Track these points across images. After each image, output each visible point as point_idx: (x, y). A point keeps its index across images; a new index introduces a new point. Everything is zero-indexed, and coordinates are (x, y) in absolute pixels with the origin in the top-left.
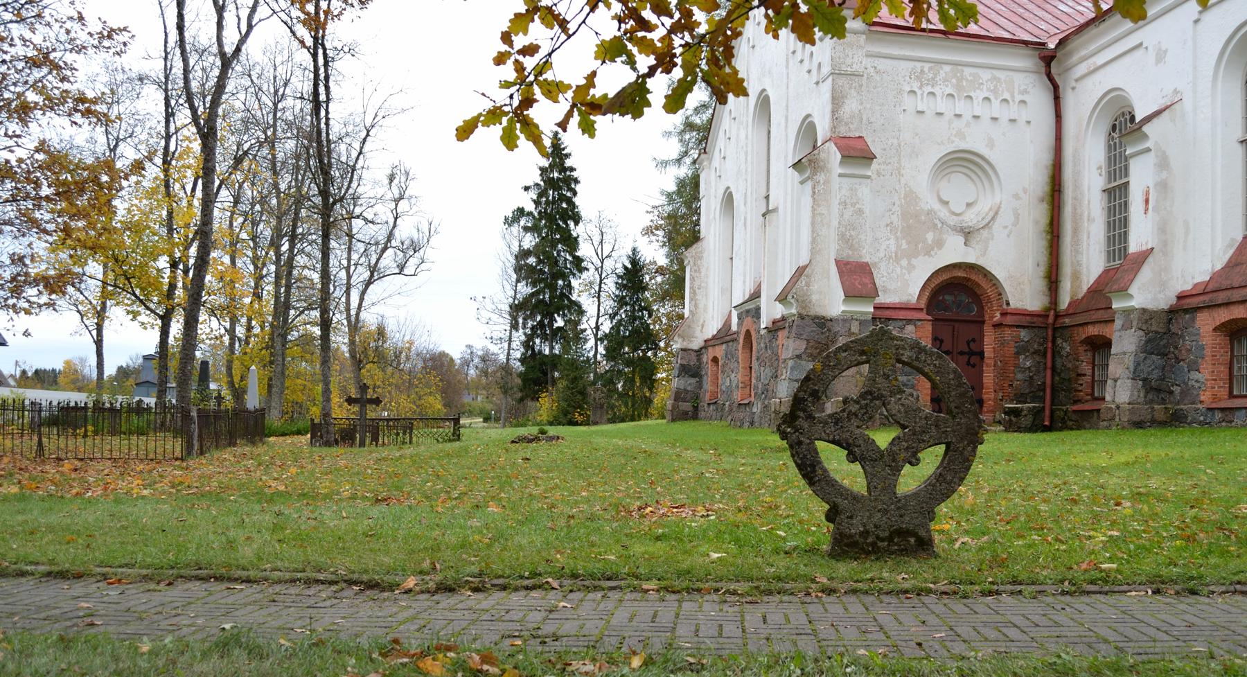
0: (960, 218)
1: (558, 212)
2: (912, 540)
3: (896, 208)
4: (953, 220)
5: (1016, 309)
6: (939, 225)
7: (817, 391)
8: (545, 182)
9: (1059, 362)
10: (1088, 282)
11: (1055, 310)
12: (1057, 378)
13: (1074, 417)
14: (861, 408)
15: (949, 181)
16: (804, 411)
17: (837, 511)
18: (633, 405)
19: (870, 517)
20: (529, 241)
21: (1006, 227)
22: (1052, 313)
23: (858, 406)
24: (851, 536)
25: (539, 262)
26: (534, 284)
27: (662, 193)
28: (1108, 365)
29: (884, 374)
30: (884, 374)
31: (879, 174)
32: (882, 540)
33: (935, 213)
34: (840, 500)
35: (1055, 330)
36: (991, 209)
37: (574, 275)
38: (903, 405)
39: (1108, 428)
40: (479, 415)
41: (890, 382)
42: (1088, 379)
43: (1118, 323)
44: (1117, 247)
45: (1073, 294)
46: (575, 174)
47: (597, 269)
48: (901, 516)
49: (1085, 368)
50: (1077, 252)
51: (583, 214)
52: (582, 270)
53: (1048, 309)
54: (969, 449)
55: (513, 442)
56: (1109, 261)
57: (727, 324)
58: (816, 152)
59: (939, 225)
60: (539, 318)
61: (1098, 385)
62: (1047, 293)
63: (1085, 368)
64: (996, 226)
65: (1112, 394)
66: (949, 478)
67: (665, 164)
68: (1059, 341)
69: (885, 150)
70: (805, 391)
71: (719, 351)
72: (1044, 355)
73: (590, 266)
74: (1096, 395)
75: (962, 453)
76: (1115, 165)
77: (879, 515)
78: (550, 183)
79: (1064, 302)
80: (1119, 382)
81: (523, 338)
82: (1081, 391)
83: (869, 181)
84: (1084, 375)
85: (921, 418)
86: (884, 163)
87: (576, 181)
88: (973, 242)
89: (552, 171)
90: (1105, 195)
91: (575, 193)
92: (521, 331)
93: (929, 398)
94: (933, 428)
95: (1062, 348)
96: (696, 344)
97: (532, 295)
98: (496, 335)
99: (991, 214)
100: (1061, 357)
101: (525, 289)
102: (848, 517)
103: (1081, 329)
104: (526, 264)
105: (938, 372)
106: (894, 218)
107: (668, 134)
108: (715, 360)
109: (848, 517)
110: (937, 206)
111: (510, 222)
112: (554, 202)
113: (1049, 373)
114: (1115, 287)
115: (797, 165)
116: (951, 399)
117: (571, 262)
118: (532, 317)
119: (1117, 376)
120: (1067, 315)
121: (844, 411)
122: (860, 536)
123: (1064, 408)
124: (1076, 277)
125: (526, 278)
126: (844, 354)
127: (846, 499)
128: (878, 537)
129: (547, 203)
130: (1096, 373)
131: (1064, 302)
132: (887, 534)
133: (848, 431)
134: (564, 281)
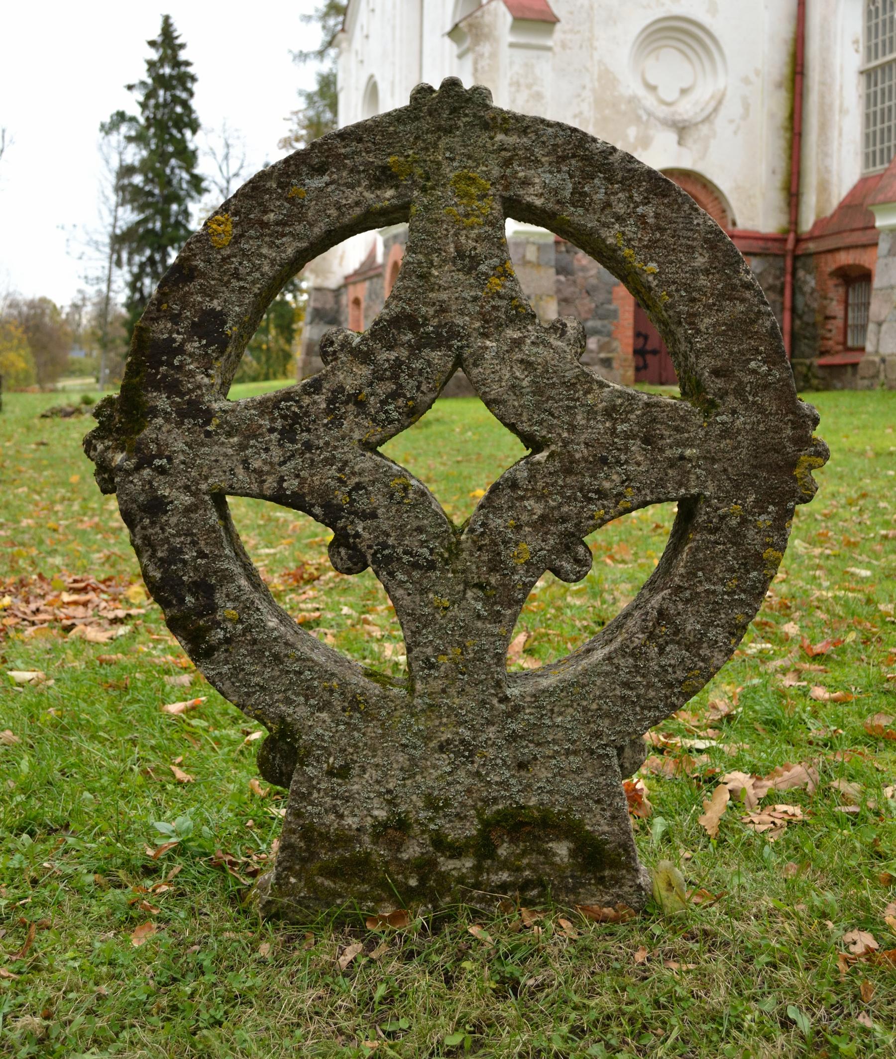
0: (672, 109)
1: (170, 118)
2: (562, 850)
3: (587, 93)
4: (662, 112)
5: (745, 231)
6: (645, 117)
7: (219, 318)
8: (154, 79)
9: (800, 302)
10: (839, 194)
11: (796, 232)
12: (798, 322)
13: (820, 373)
14: (378, 377)
15: (657, 59)
16: (173, 388)
17: (294, 751)
18: (268, 360)
19: (409, 772)
20: (134, 155)
21: (731, 121)
22: (791, 237)
23: (365, 371)
24: (344, 839)
25: (147, 181)
26: (141, 209)
27: (300, 93)
28: (869, 304)
29: (461, 254)
30: (461, 254)
31: (564, 46)
32: (456, 851)
33: (639, 101)
34: (302, 711)
35: (796, 258)
36: (712, 97)
37: (192, 198)
38: (527, 364)
39: (870, 388)
40: (90, 374)
41: (482, 280)
42: (839, 322)
43: (884, 246)
44: (878, 147)
45: (820, 209)
46: (191, 70)
47: (221, 191)
48: (522, 766)
49: (835, 308)
50: (825, 155)
51: (202, 120)
52: (201, 191)
53: (787, 232)
54: (764, 521)
55: (44, 416)
56: (867, 165)
57: (372, 255)
58: (479, 13)
59: (645, 117)
60: (148, 252)
61: (853, 331)
62: (786, 209)
63: (835, 308)
64: (720, 121)
65: (875, 342)
66: (692, 625)
67: (303, 56)
68: (801, 274)
69: (571, 13)
70: (175, 319)
71: (361, 290)
72: (782, 292)
73: (212, 187)
74: (850, 343)
75: (737, 538)
76: (876, 37)
77: (444, 762)
78: (161, 81)
79: (808, 222)
80: (884, 327)
81: (129, 278)
82: (829, 339)
83: (549, 54)
84: (834, 318)
85: (591, 413)
86: (571, 31)
87: (193, 79)
88: (689, 142)
89: (162, 66)
90: (863, 79)
91: (191, 94)
92: (126, 268)
93: (630, 350)
94: (635, 446)
95: (805, 282)
96: (333, 282)
97: (139, 223)
98: (93, 274)
99: (713, 104)
100: (804, 294)
101: (128, 216)
102: (330, 773)
103: (829, 257)
104: (131, 184)
105: (652, 245)
106: (585, 107)
107: (308, 18)
108: (357, 302)
109: (330, 773)
110: (641, 92)
111: (108, 129)
112: (165, 105)
113: (787, 316)
114: (881, 197)
115: (455, 33)
116: (700, 343)
117: (188, 182)
118: (139, 251)
119: (882, 318)
120: (811, 238)
121: (314, 387)
122: (376, 837)
123: (808, 361)
124: (824, 187)
125: (132, 201)
126: (317, 183)
127: (325, 706)
128: (439, 842)
129: (157, 106)
130: (850, 315)
131: (808, 222)
132: (472, 829)
133: (330, 461)
134: (180, 205)
